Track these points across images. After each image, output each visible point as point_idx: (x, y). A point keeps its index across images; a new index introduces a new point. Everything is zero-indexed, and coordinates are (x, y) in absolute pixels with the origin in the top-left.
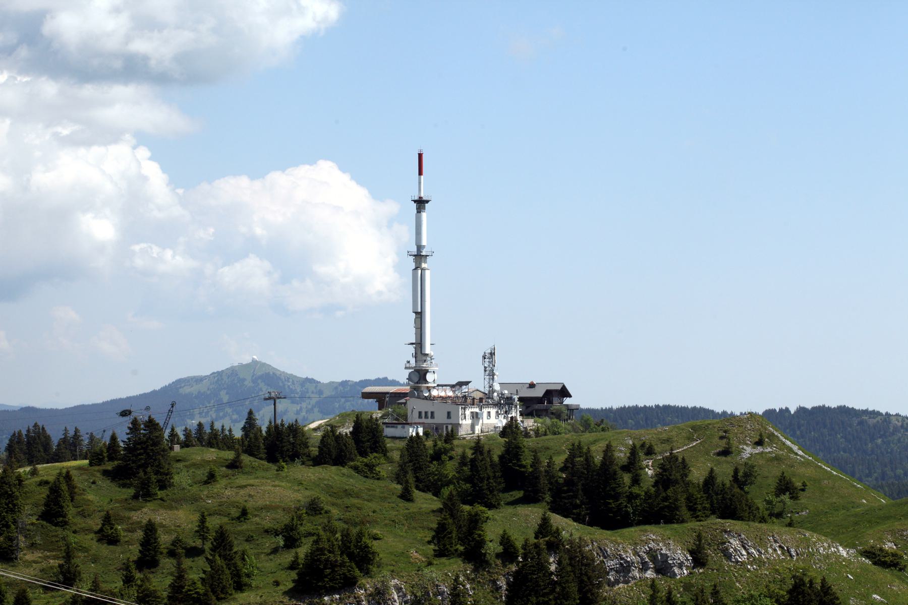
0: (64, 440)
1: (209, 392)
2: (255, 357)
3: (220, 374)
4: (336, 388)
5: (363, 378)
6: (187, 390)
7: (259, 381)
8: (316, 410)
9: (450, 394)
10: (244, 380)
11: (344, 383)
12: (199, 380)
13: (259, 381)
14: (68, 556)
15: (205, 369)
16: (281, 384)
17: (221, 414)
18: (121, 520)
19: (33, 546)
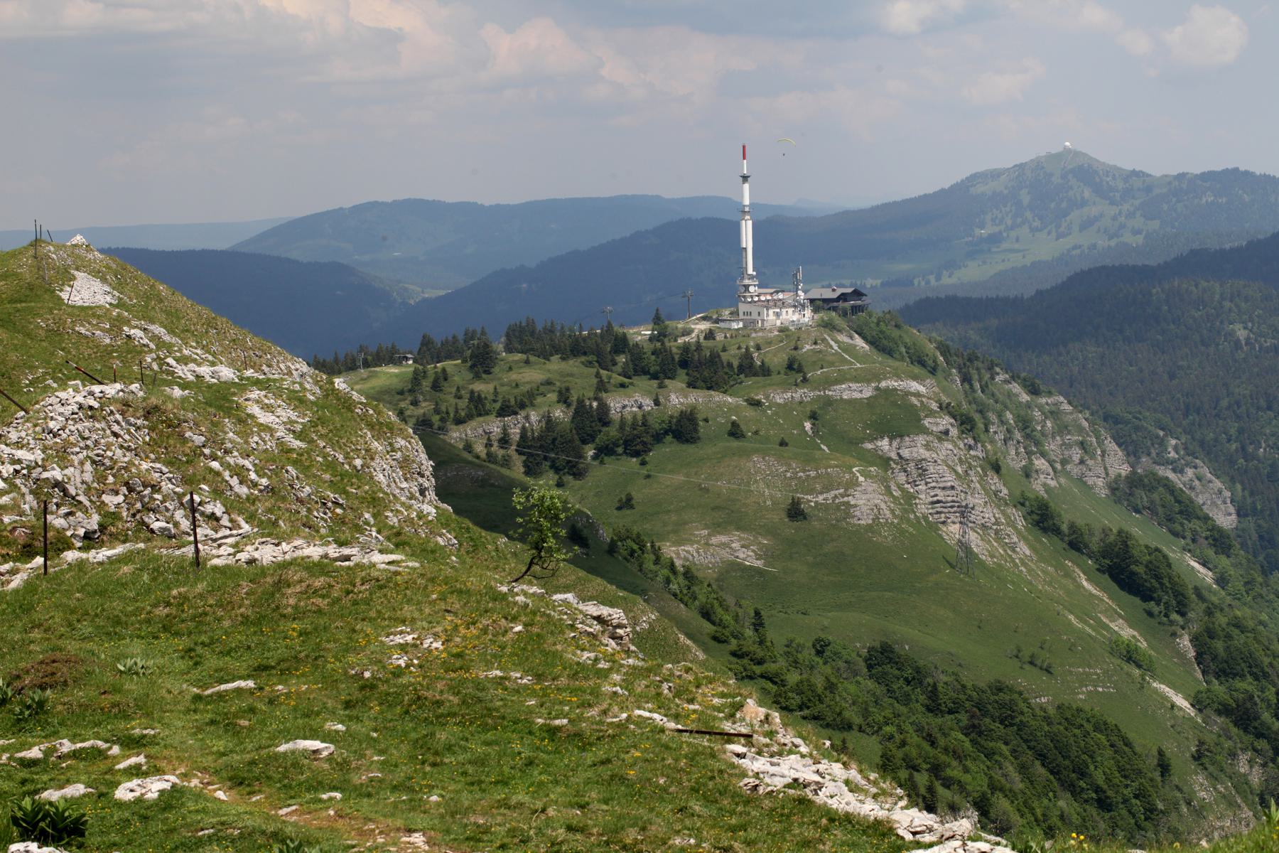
0: (545, 329)
1: (1006, 192)
2: (1067, 144)
3: (1021, 167)
4: (1170, 183)
5: (1206, 170)
6: (980, 189)
7: (1070, 176)
8: (1138, 214)
9: (769, 297)
10: (1051, 175)
11: (1181, 177)
12: (995, 175)
13: (1070, 176)
14: (437, 404)
15: (1006, 159)
16: (1097, 180)
17: (1019, 220)
18: (464, 388)
19: (425, 400)
